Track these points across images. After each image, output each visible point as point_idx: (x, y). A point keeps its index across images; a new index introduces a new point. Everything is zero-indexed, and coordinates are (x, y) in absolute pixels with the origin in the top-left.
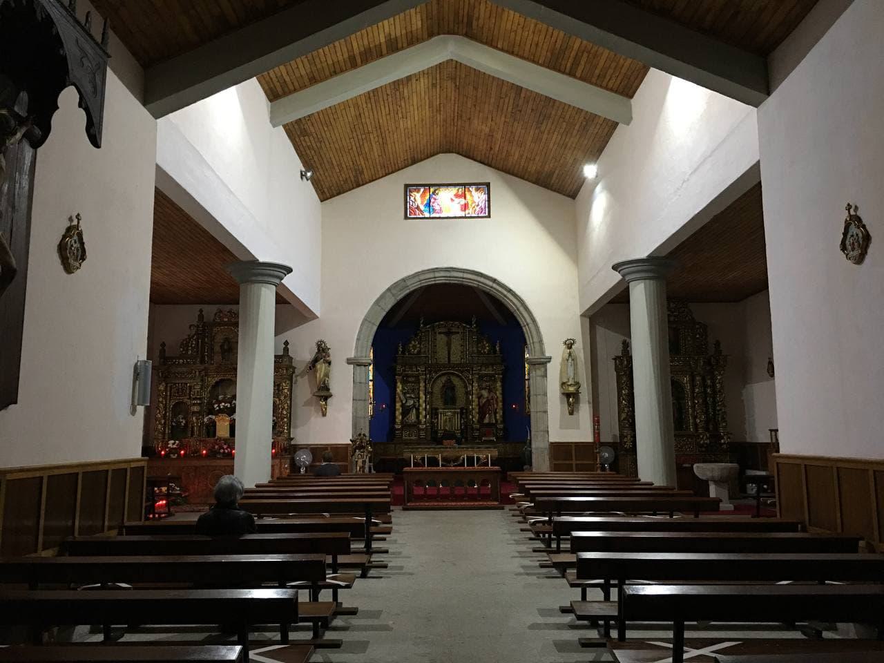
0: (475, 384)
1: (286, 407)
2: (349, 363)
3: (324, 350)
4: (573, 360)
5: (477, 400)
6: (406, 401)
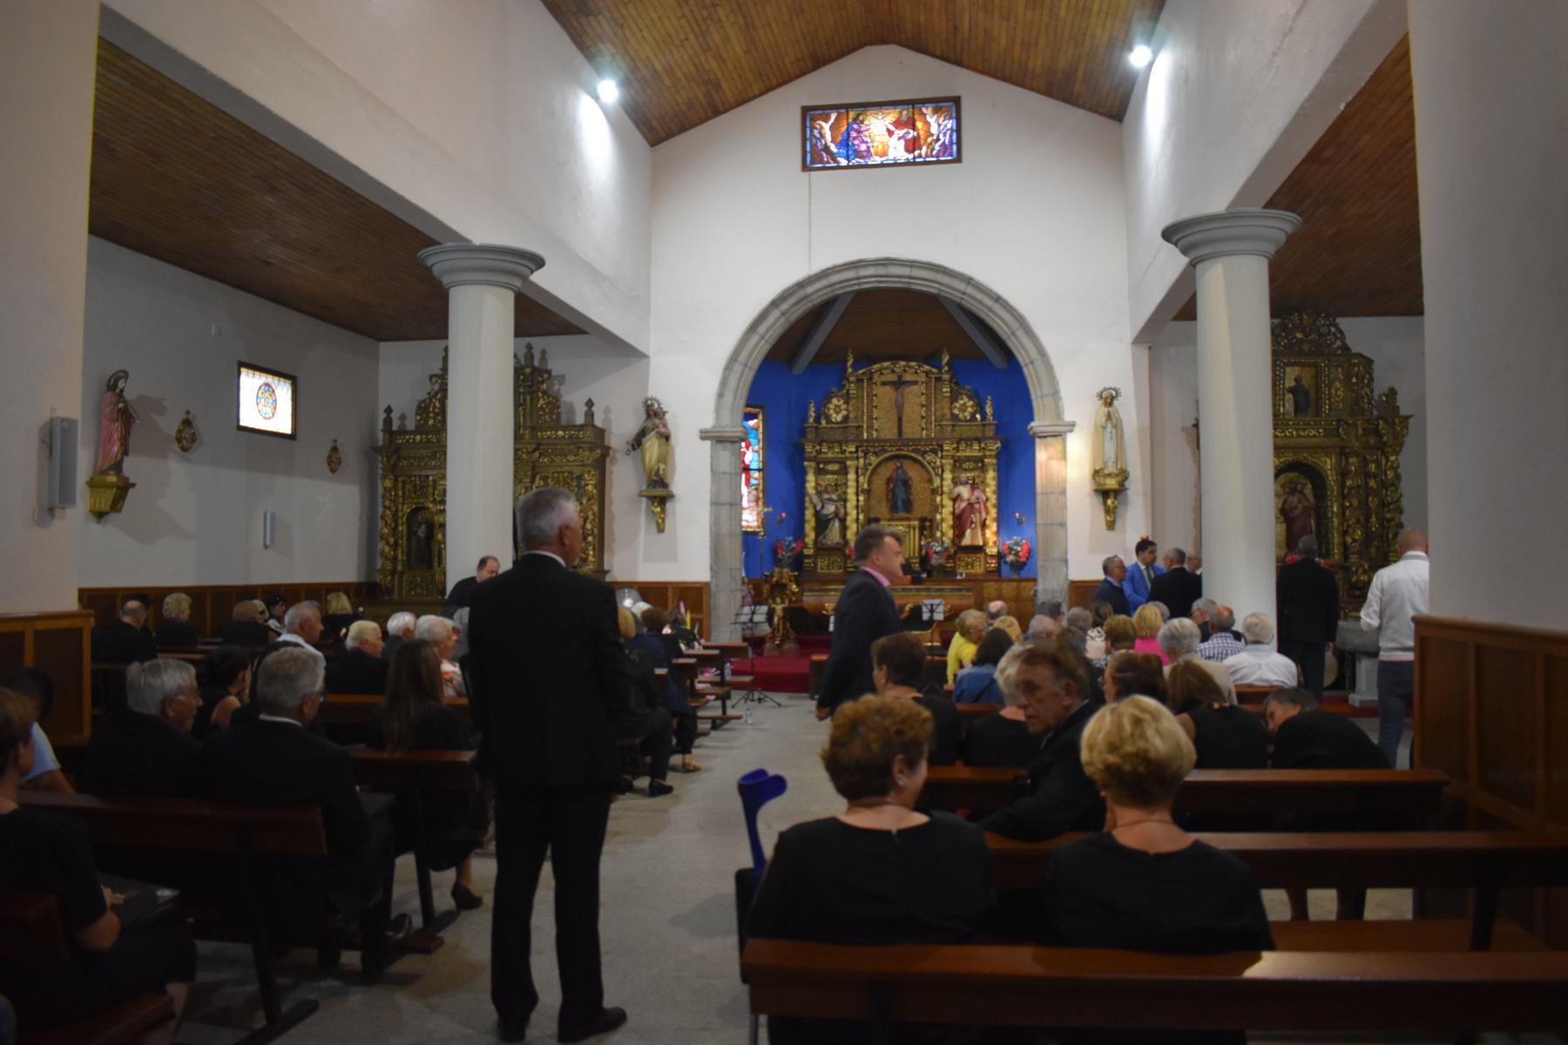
0: (948, 476)
1: (591, 517)
2: (703, 438)
3: (656, 414)
4: (1115, 427)
5: (951, 503)
6: (823, 507)
